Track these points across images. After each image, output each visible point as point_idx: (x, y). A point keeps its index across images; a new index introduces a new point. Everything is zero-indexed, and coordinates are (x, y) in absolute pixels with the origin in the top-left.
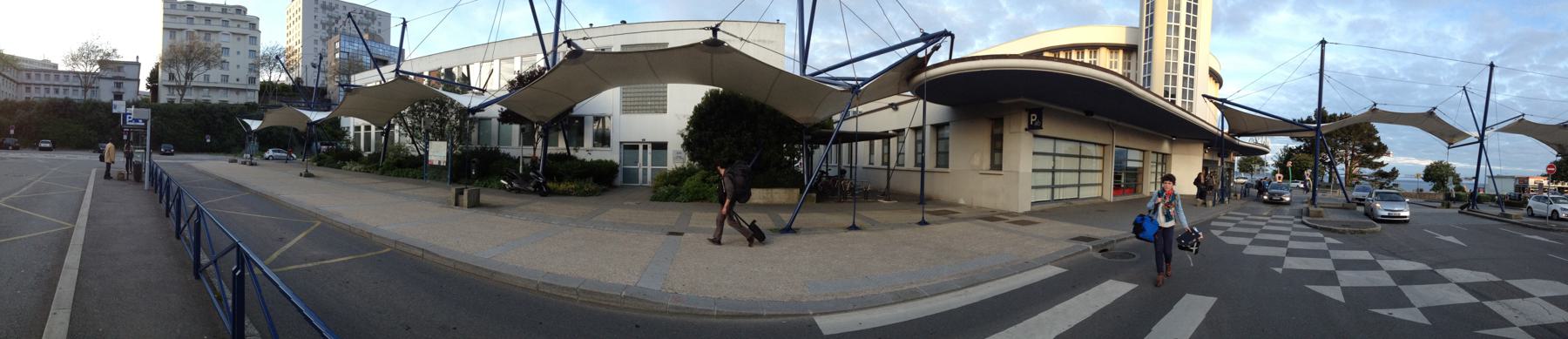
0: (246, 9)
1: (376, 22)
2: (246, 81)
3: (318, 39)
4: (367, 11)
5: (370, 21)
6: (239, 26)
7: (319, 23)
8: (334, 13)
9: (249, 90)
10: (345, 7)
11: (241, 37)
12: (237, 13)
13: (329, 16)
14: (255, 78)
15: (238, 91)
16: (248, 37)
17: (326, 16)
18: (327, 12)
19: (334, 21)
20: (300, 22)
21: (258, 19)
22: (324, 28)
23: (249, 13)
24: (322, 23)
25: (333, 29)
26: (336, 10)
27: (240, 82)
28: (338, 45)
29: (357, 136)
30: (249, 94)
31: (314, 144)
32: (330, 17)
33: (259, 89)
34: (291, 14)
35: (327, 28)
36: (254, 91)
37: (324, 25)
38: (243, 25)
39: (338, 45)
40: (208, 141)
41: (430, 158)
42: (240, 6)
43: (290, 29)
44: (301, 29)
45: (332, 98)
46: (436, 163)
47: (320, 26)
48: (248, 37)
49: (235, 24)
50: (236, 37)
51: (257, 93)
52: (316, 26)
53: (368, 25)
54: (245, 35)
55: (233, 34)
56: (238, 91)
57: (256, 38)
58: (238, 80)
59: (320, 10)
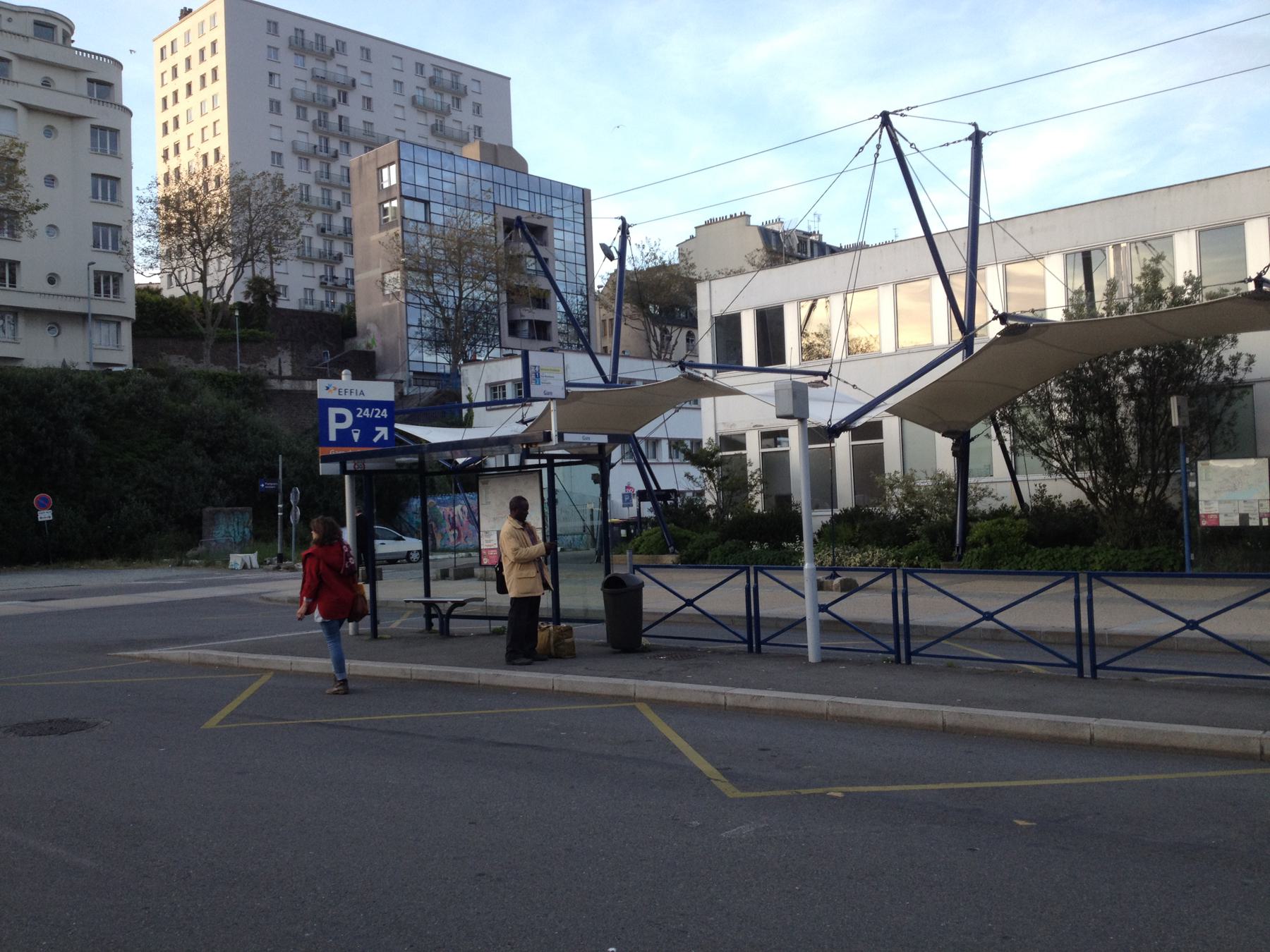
0: (71, 27)
1: (467, 104)
2: (84, 286)
3: (284, 149)
4: (437, 69)
5: (448, 99)
6: (46, 83)
7: (283, 97)
8: (332, 68)
9: (100, 319)
10: (420, 68)
11: (59, 125)
12: (38, 35)
13: (315, 78)
14: (118, 277)
15: (55, 319)
16: (85, 128)
17: (306, 75)
18: (311, 63)
19: (332, 93)
20: (220, 88)
21: (119, 65)
22: (301, 114)
23: (80, 40)
24: (293, 99)
25: (333, 119)
26: (339, 58)
27: (59, 289)
28: (390, 176)
29: (774, 465)
30: (101, 334)
31: (416, 503)
32: (321, 80)
33: (132, 314)
34: (179, 59)
35: (313, 114)
36: (117, 321)
37: (301, 106)
38: (61, 80)
39: (390, 176)
40: (45, 515)
41: (1203, 509)
42: (47, 13)
43: (173, 111)
44: (222, 114)
45: (377, 349)
46: (1230, 520)
47: (289, 109)
48: (85, 128)
49: (37, 74)
50: (41, 122)
51: (127, 329)
52: (275, 106)
53: (444, 112)
54: (73, 118)
55: (30, 109)
56: (55, 319)
57: (115, 132)
58: (52, 280)
59: (287, 58)
